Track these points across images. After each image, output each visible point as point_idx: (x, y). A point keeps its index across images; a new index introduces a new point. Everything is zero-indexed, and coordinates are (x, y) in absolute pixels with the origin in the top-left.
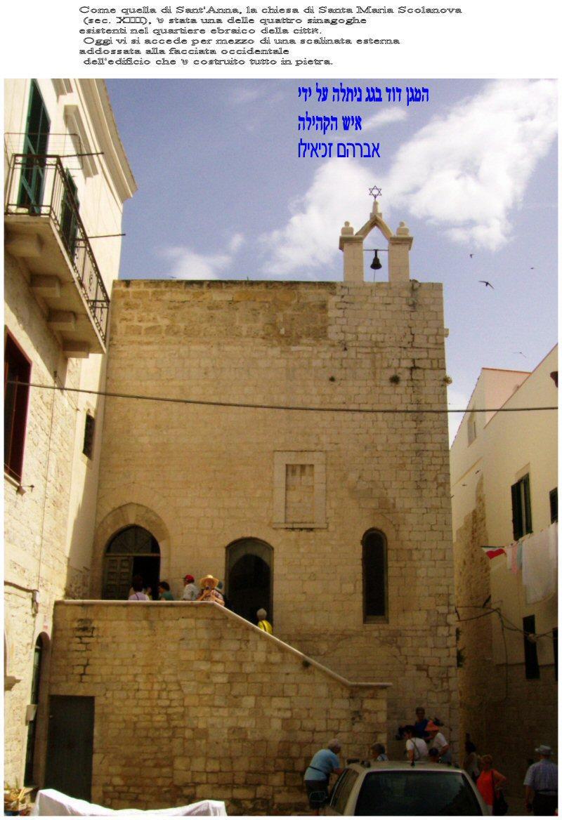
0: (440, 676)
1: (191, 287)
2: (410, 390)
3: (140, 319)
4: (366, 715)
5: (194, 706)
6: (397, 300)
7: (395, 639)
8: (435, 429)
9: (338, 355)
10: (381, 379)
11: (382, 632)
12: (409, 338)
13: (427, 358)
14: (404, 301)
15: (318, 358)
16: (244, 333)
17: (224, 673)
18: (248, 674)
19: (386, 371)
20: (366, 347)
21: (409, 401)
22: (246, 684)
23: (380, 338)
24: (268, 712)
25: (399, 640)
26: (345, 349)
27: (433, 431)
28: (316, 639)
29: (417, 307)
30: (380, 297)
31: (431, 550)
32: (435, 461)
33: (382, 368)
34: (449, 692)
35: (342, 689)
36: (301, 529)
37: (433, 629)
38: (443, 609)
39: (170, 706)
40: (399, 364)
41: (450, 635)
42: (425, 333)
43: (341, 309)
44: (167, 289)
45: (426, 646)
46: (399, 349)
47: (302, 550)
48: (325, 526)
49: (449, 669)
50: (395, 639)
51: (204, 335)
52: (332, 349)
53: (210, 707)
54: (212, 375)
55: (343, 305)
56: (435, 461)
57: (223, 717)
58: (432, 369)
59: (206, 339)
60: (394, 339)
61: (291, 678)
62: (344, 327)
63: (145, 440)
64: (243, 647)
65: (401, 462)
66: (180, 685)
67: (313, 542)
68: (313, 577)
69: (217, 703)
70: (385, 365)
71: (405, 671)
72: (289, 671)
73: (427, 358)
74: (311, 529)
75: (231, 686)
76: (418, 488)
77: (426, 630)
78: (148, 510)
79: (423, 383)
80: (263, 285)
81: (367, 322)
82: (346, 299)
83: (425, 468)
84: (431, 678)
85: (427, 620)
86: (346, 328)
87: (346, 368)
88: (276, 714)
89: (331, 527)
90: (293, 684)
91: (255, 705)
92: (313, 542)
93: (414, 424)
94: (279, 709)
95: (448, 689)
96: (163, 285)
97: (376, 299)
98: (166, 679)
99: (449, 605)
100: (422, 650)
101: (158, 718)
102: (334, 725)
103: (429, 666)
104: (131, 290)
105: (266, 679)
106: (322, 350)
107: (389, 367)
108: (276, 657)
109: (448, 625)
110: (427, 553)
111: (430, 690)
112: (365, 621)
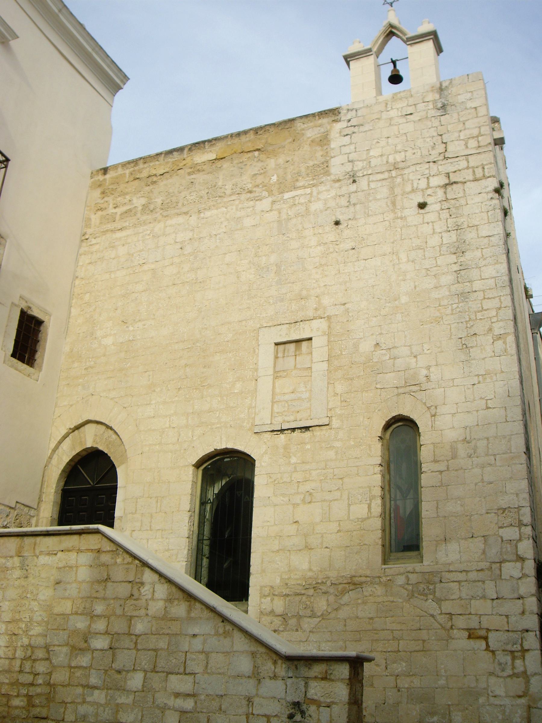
0: (509, 647)
1: (171, 156)
2: (445, 214)
3: (115, 206)
4: (313, 708)
5: (63, 686)
6: (421, 106)
7: (431, 587)
8: (485, 259)
9: (344, 190)
10: (403, 208)
11: (411, 576)
12: (441, 148)
13: (468, 168)
14: (431, 106)
15: (319, 199)
16: (228, 192)
17: (107, 633)
18: (138, 636)
19: (412, 196)
20: (382, 173)
21: (445, 228)
22: (134, 651)
23: (399, 157)
24: (162, 699)
25: (437, 590)
26: (354, 181)
27: (482, 263)
29: (448, 108)
30: (398, 109)
31: (488, 439)
32: (487, 304)
33: (404, 193)
35: (275, 663)
36: (293, 430)
37: (494, 566)
38: (511, 533)
39: (32, 684)
40: (428, 183)
41: (525, 576)
42: (462, 138)
43: (347, 135)
44: (146, 165)
45: (484, 597)
46: (427, 166)
47: (293, 460)
48: (326, 421)
49: (525, 634)
50: (431, 587)
51: (183, 205)
52: (337, 185)
53: (83, 686)
54: (188, 249)
55: (349, 131)
56: (487, 304)
57: (96, 704)
58: (476, 180)
59: (185, 209)
60: (419, 154)
61: (197, 644)
62: (350, 155)
63: (109, 341)
64: (136, 593)
65: (438, 314)
66: (48, 652)
67: (308, 446)
68: (309, 498)
69: (93, 681)
70: (408, 188)
73: (468, 168)
74: (307, 428)
75: (114, 655)
76: (465, 347)
77: (482, 570)
79: (463, 202)
80: (251, 132)
81: (383, 143)
82: (354, 122)
83: (473, 317)
84: (493, 652)
85: (484, 552)
86: (352, 156)
87: (354, 205)
89: (335, 423)
90: (202, 652)
91: (143, 685)
92: (308, 446)
93: (453, 258)
94: (177, 695)
96: (141, 163)
97: (393, 113)
98: (33, 642)
101: (16, 702)
103: (488, 630)
104: (108, 176)
105: (162, 644)
106: (324, 189)
107: (413, 191)
108: (180, 609)
109: (521, 559)
110: (482, 444)
111: (491, 674)
112: (385, 561)
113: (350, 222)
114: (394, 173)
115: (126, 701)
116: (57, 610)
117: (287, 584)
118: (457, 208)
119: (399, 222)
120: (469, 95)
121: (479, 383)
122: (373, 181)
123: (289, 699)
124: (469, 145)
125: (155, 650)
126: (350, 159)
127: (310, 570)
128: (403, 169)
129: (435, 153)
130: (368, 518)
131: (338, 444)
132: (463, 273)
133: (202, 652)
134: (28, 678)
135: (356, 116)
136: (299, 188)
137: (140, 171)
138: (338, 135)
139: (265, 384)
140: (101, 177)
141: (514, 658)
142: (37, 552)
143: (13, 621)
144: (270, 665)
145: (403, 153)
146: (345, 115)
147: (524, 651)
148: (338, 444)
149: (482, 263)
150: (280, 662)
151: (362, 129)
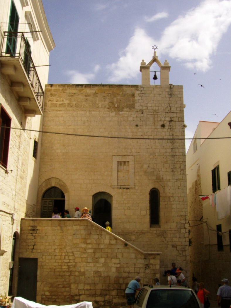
0: (182, 249)
1: (78, 87)
2: (169, 130)
6: (164, 92)
9: (139, 115)
10: (157, 126)
11: (158, 231)
12: (169, 108)
13: (177, 117)
16: (100, 106)
19: (159, 122)
20: (151, 112)
22: (101, 253)
23: (157, 108)
24: (110, 265)
26: (142, 113)
27: (179, 147)
28: (130, 234)
29: (172, 95)
32: (180, 160)
33: (158, 121)
34: (186, 256)
35: (141, 255)
36: (124, 188)
38: (183, 222)
39: (69, 262)
40: (165, 119)
41: (186, 233)
43: (141, 96)
44: (68, 88)
45: (176, 237)
46: (165, 113)
48: (134, 187)
50: (163, 234)
52: (137, 113)
53: (86, 262)
55: (141, 95)
56: (180, 160)
58: (178, 121)
60: (163, 109)
61: (120, 251)
63: (59, 151)
64: (100, 238)
66: (73, 253)
67: (129, 193)
68: (129, 208)
69: (89, 261)
70: (159, 120)
71: (167, 247)
72: (119, 247)
74: (128, 188)
75: (95, 254)
77: (176, 231)
78: (60, 180)
82: (143, 92)
83: (176, 163)
84: (178, 251)
85: (176, 226)
87: (142, 121)
88: (113, 265)
89: (137, 188)
90: (121, 253)
92: (129, 193)
93: (171, 144)
94: (115, 264)
95: (185, 255)
97: (155, 92)
99: (186, 220)
100: (175, 239)
101: (64, 267)
102: (137, 270)
103: (177, 245)
104: (53, 88)
107: (160, 120)
108: (113, 242)
109: (185, 228)
110: (177, 198)
111: (178, 256)
112: (151, 226)
113: (141, 127)
114: (155, 113)
115: (100, 266)
116: (75, 242)
117: (123, 232)
118: (173, 129)
119: (156, 130)
120: (179, 93)
121: (176, 181)
122: (148, 114)
123: (145, 263)
124: (178, 110)
125: (108, 253)
126: (141, 105)
127: (130, 228)
128: (157, 112)
129: (168, 109)
130: (146, 215)
131: (137, 194)
132: (173, 149)
133: (121, 253)
134: (68, 261)
135: (144, 90)
136: (125, 111)
137: (66, 90)
138: (138, 95)
139: (115, 174)
140: (49, 88)
141: (183, 252)
142: (66, 225)
143: (59, 245)
144: (140, 256)
145: (158, 107)
146: (140, 89)
147: (185, 250)
148: (137, 194)
149: (179, 147)
150: (142, 255)
151: (145, 95)
